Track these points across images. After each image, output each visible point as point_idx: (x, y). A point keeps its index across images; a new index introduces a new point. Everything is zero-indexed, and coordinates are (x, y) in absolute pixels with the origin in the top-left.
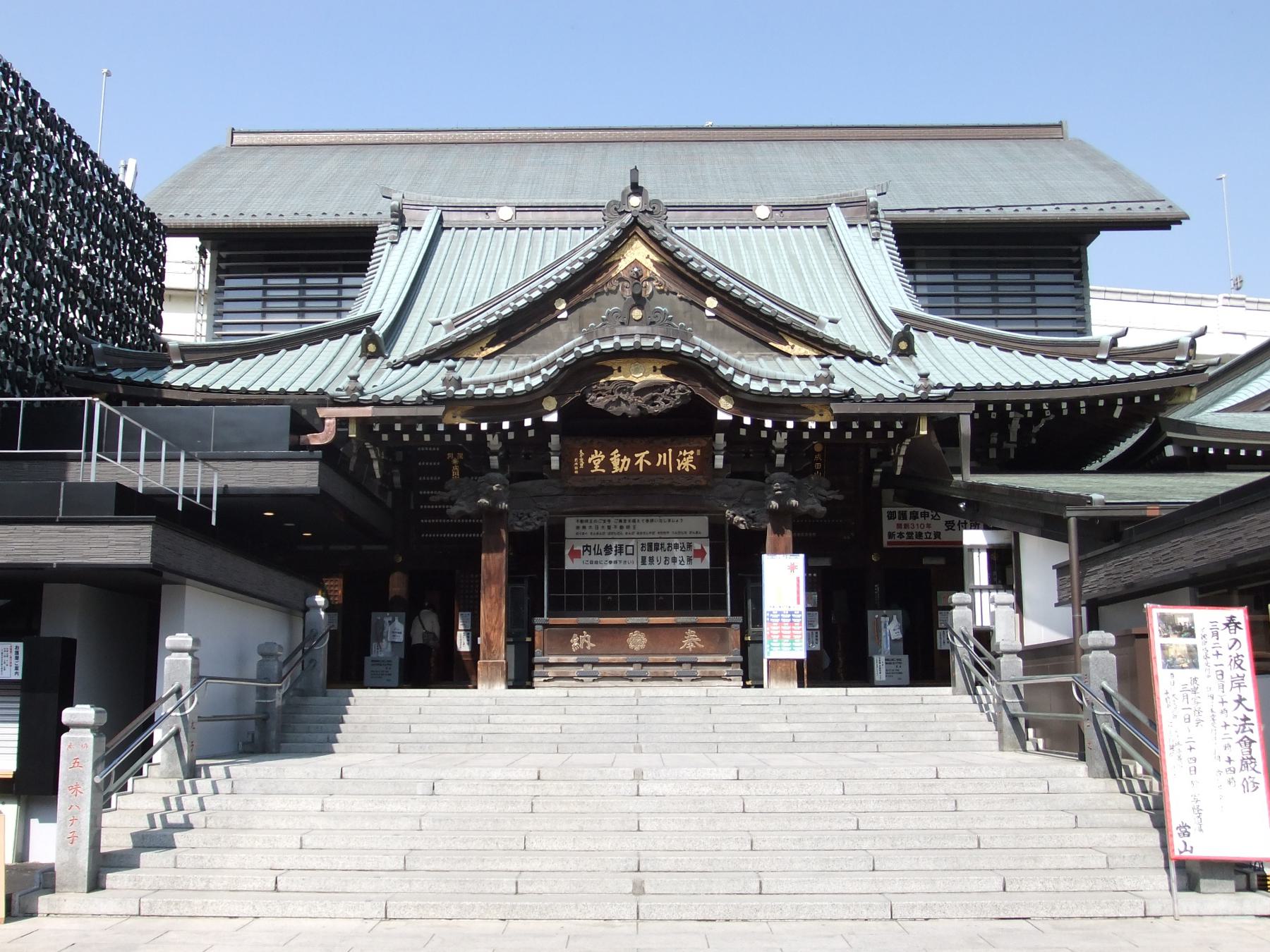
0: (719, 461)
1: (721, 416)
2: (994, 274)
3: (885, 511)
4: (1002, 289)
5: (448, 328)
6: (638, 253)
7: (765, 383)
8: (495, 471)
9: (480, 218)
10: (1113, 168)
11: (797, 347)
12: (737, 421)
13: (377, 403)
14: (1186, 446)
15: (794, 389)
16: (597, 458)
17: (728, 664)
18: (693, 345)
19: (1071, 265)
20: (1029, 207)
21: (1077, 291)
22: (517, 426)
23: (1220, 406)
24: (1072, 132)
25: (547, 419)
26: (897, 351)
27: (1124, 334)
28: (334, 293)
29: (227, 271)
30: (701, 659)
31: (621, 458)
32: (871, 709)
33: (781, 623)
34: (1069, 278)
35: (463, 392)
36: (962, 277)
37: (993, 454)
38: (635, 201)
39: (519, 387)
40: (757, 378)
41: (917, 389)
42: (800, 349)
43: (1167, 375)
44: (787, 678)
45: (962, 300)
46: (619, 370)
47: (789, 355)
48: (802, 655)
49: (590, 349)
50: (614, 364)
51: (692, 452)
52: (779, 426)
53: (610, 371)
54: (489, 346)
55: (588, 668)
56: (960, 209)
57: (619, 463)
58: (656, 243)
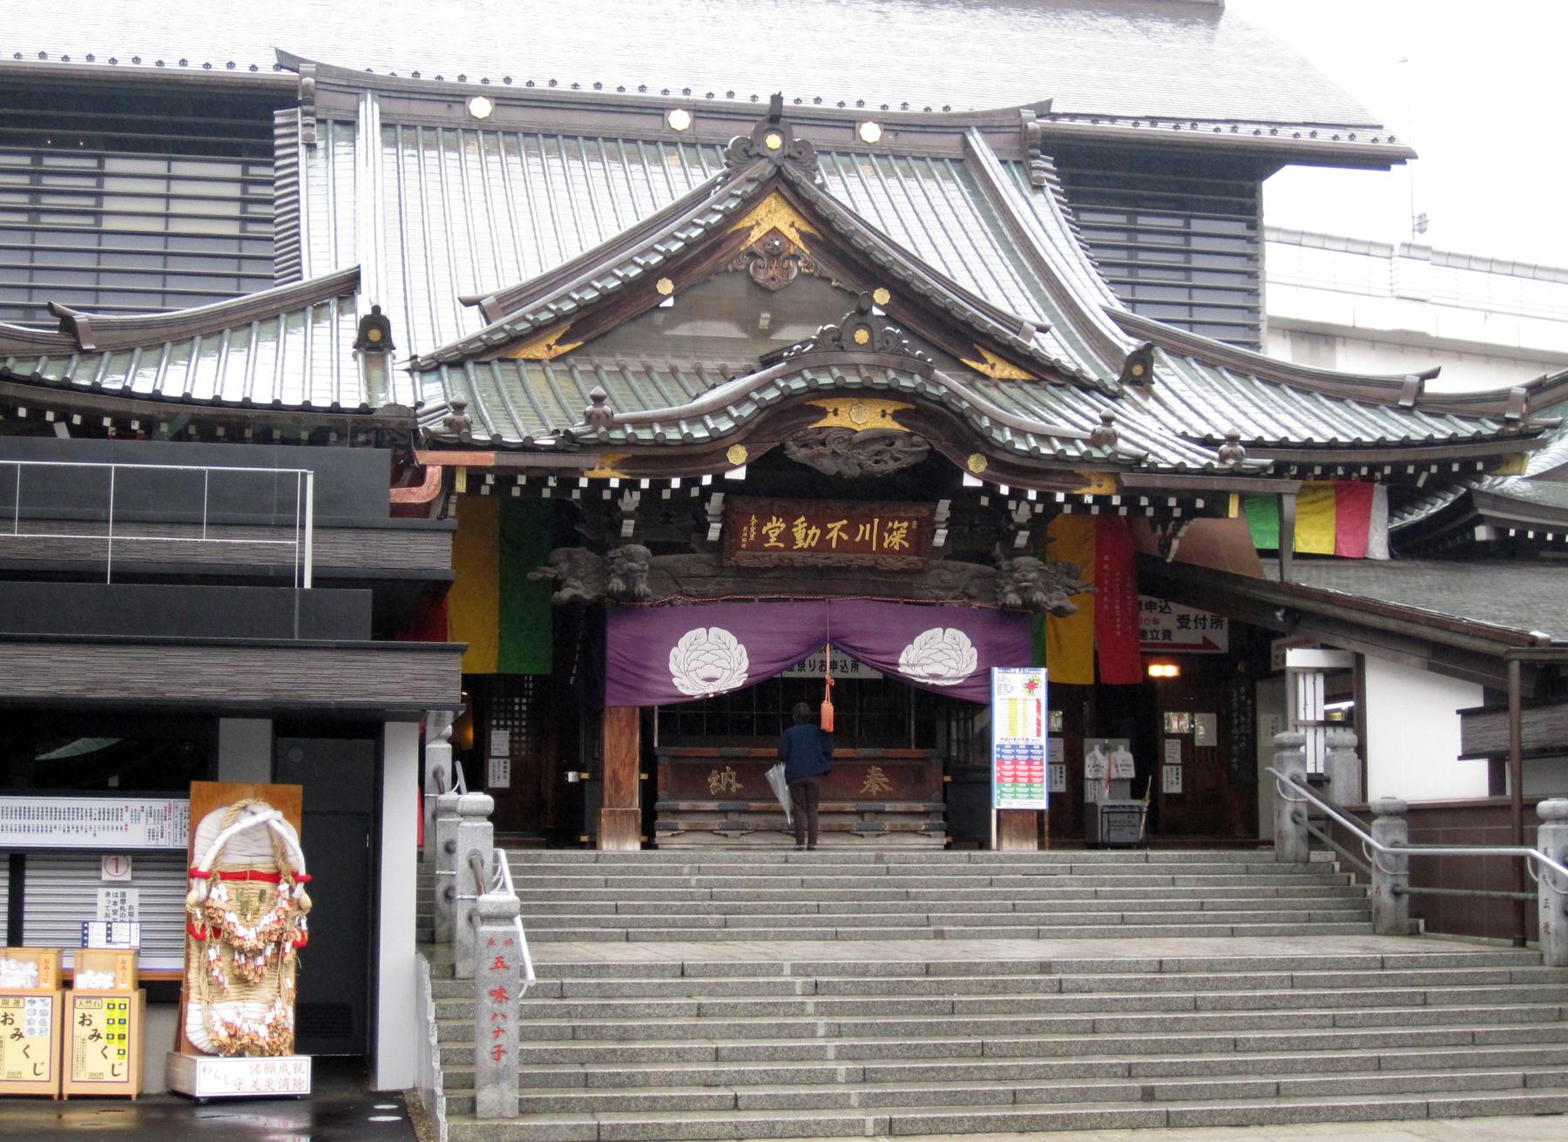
0: (940, 538)
1: (969, 481)
9: (438, 110)
13: (496, 445)
14: (1500, 529)
16: (774, 527)
17: (926, 814)
21: (1249, 249)
25: (729, 475)
28: (90, 183)
30: (889, 806)
31: (808, 528)
33: (1015, 762)
42: (1003, 370)
43: (1496, 438)
44: (1022, 835)
46: (836, 413)
48: (1042, 804)
51: (905, 524)
52: (1017, 494)
53: (823, 413)
54: (559, 342)
55: (734, 818)
57: (804, 534)
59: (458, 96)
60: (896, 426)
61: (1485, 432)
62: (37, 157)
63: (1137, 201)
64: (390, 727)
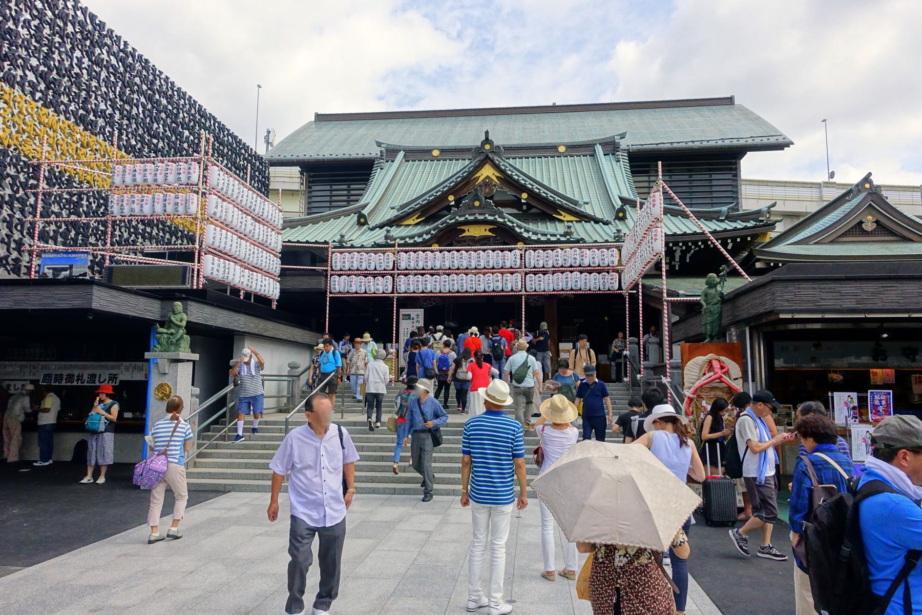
2: (690, 176)
5: (398, 210)
6: (487, 172)
10: (757, 119)
11: (567, 215)
14: (767, 262)
19: (731, 169)
20: (708, 141)
23: (788, 242)
26: (617, 218)
27: (774, 205)
29: (313, 182)
34: (730, 176)
38: (487, 147)
40: (527, 231)
42: (569, 217)
56: (672, 143)
58: (496, 167)
59: (429, 151)
60: (490, 234)
61: (739, 227)
64: (235, 337)
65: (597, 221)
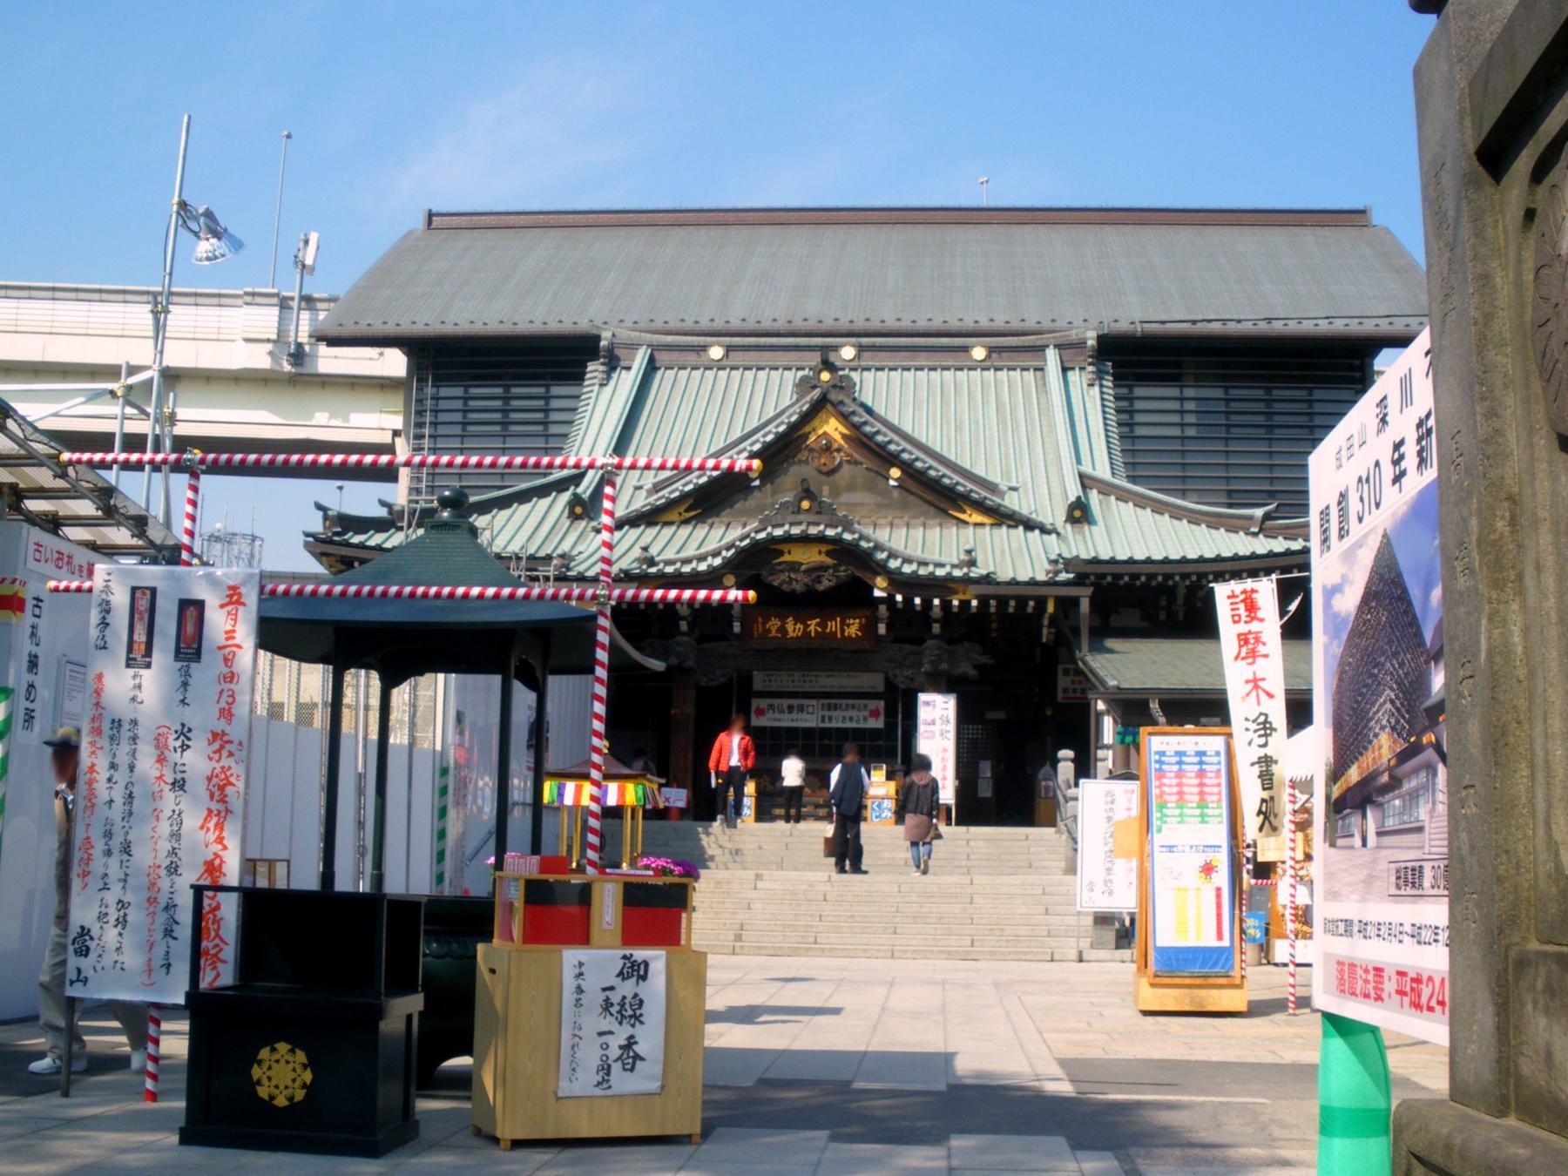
0: (882, 629)
1: (877, 593)
2: (1268, 390)
3: (1061, 668)
4: (1278, 407)
6: (832, 428)
7: (914, 567)
8: (684, 634)
12: (891, 597)
15: (940, 572)
18: (853, 532)
22: (908, 601)
24: (1377, 218)
32: (981, 843)
33: (1180, 774)
35: (653, 570)
36: (1234, 393)
37: (1162, 616)
39: (703, 567)
41: (1048, 572)
42: (977, 518)
45: (1233, 417)
47: (966, 523)
49: (762, 535)
50: (785, 547)
53: (782, 553)
54: (687, 511)
57: (793, 629)
58: (845, 418)
62: (507, 388)
63: (1272, 379)
65: (1029, 525)
